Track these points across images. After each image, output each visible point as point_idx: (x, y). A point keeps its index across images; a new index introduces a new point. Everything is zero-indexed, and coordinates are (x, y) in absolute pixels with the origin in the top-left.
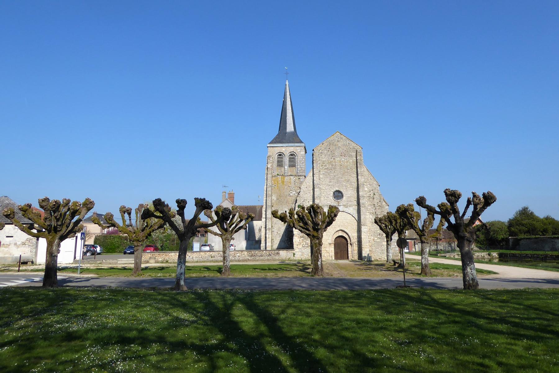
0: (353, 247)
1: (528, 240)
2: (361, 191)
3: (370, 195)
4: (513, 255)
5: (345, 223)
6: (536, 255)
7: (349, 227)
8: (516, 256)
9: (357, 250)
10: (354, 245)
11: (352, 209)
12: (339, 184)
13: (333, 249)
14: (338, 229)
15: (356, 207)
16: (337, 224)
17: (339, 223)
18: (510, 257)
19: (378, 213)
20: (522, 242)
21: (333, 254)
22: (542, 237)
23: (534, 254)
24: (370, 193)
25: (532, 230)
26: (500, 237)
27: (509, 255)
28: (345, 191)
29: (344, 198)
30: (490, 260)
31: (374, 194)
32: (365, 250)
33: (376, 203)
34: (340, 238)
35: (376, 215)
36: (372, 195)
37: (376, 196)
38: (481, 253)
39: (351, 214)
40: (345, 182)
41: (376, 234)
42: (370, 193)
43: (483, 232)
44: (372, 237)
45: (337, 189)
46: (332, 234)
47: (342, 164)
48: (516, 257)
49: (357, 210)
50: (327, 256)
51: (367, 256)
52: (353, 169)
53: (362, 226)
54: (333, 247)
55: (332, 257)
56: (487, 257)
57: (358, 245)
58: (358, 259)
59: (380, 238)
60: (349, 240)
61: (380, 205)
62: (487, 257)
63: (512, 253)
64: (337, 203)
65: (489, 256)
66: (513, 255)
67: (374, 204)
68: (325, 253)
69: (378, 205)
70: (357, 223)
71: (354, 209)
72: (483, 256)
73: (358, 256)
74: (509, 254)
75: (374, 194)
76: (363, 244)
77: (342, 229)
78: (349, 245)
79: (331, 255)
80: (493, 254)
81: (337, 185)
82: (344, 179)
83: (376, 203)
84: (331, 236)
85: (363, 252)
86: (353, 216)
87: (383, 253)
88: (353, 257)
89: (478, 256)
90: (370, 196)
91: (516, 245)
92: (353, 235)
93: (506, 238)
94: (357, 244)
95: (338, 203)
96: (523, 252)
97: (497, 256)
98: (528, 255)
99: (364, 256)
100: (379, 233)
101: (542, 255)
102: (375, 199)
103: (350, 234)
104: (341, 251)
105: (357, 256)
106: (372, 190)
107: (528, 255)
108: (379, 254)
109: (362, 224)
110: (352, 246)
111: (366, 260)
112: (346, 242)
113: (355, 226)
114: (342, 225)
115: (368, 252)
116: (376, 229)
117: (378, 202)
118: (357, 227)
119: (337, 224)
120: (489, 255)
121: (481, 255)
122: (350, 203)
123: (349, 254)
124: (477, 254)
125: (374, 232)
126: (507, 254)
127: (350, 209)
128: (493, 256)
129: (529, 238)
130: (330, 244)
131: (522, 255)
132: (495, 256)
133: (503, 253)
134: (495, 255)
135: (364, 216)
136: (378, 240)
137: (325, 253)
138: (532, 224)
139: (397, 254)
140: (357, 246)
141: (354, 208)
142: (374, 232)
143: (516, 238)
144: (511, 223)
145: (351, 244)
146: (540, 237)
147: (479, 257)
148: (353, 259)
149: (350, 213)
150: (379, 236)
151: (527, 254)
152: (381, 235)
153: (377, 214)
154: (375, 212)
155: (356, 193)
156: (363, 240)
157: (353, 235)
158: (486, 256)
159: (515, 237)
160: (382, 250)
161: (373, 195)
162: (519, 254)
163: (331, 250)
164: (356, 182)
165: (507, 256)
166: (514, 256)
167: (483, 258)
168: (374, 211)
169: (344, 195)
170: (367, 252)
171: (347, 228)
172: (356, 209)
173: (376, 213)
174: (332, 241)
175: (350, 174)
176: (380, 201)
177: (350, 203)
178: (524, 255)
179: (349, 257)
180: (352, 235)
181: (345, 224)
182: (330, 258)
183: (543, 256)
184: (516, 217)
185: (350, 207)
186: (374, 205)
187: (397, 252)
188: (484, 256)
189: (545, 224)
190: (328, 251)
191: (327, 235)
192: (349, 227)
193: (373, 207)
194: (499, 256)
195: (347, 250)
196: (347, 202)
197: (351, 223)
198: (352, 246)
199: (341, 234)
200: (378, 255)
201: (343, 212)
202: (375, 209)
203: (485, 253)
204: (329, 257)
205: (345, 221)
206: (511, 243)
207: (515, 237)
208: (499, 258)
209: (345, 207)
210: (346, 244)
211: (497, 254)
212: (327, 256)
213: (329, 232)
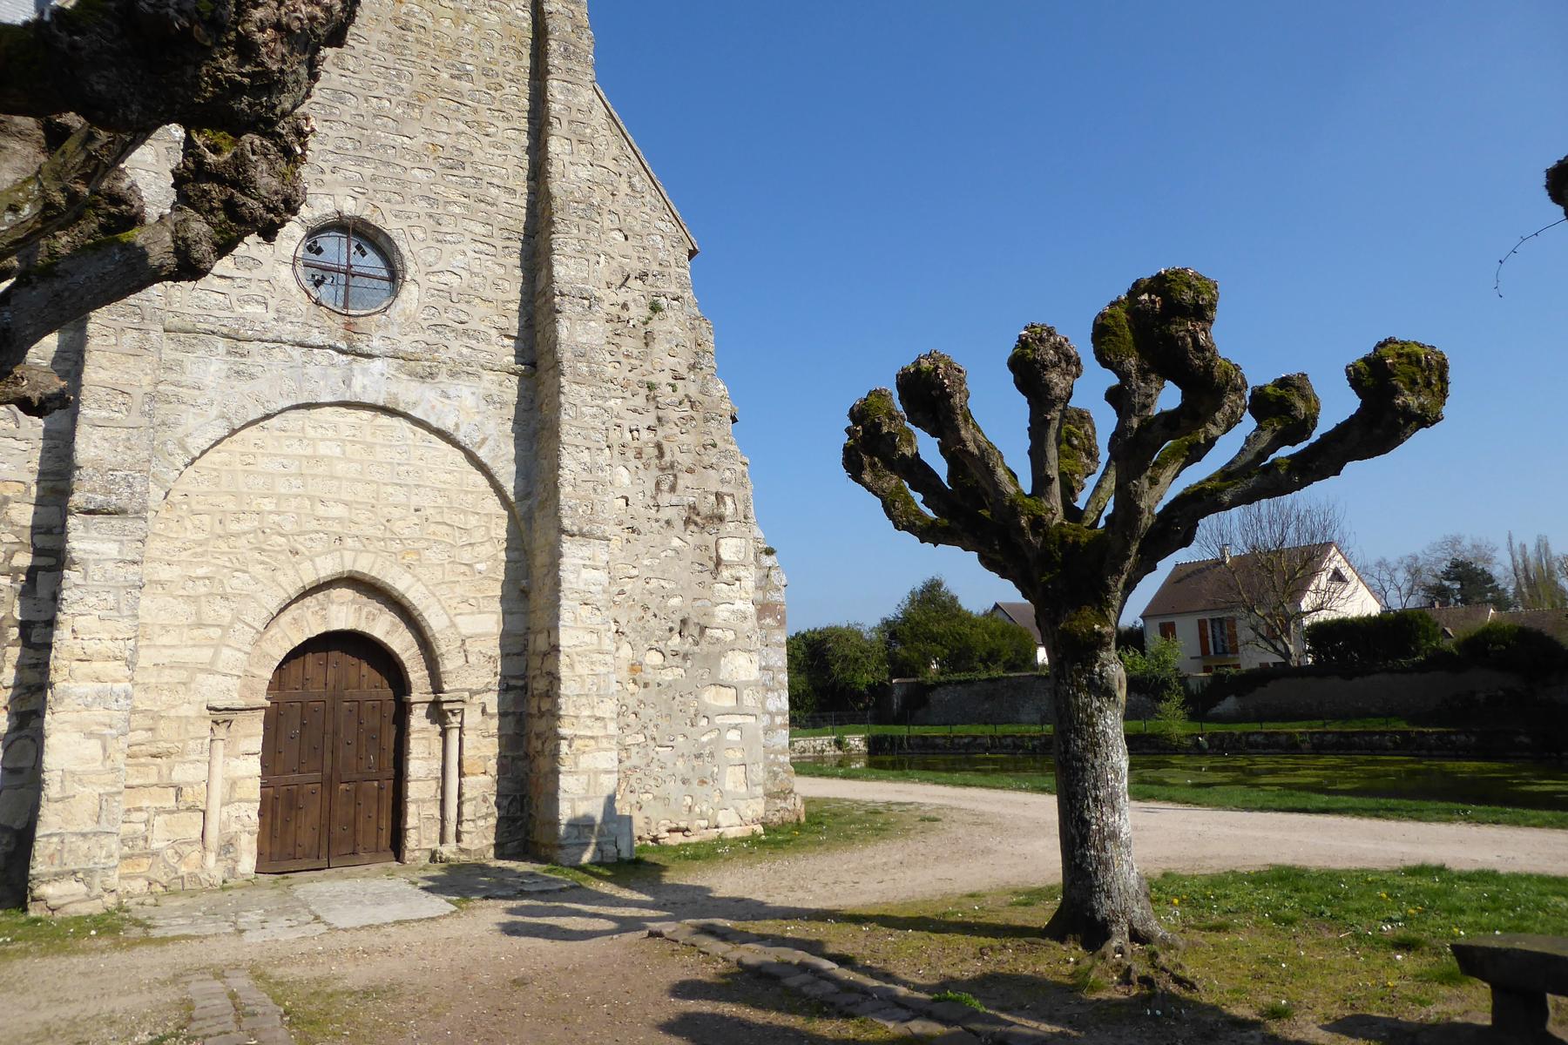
0: (454, 736)
1: (959, 688)
2: (567, 250)
3: (625, 306)
4: (921, 742)
5: (396, 513)
6: (1009, 741)
7: (432, 556)
8: (936, 746)
9: (492, 766)
10: (472, 717)
11: (469, 401)
12: (368, 171)
13: (254, 766)
14: (328, 568)
15: (510, 390)
16: (314, 525)
17: (338, 511)
18: (910, 751)
19: (679, 457)
20: (934, 697)
21: (250, 813)
22: (1015, 677)
23: (1005, 737)
24: (623, 296)
25: (959, 657)
26: (865, 679)
27: (908, 743)
28: (419, 234)
29: (411, 295)
30: (840, 765)
31: (655, 308)
32: (585, 762)
33: (664, 379)
34: (335, 655)
35: (663, 469)
36: (638, 312)
37: (665, 326)
38: (815, 741)
39: (460, 436)
40: (429, 163)
41: (653, 622)
42: (623, 296)
43: (800, 665)
44: (626, 651)
45: (350, 208)
46: (257, 617)
47: (408, 13)
48: (934, 748)
49: (511, 412)
50: (178, 845)
51: (599, 819)
52: (506, 84)
53: (568, 546)
54: (256, 744)
55: (228, 847)
56: (831, 751)
57: (502, 715)
58: (499, 855)
59: (685, 657)
60: (417, 675)
61: (693, 391)
62: (832, 753)
63: (917, 737)
64: (341, 332)
65: (840, 749)
66: (921, 742)
67: (653, 379)
68: (160, 811)
69: (681, 393)
70: (504, 523)
71: (488, 399)
72: (819, 748)
73: (500, 820)
74: (909, 738)
75: (655, 308)
76: (566, 706)
77: (365, 565)
78: (418, 720)
79: (224, 825)
80: (852, 742)
81: (351, 169)
82: (423, 138)
83: (664, 379)
84: (244, 636)
85: (565, 782)
86: (482, 454)
87: (703, 782)
88: (451, 829)
89: (804, 752)
90: (625, 315)
91: (918, 702)
92: (467, 625)
93: (881, 684)
94: (493, 708)
95: (348, 326)
96: (960, 730)
97: (862, 747)
98: (979, 741)
99: (573, 824)
100: (677, 618)
101: (1032, 738)
102: (660, 347)
103: (435, 621)
104: (329, 783)
105: (493, 821)
106: (642, 276)
107: (979, 741)
108: (673, 787)
109: (566, 523)
110: (444, 734)
111: (586, 857)
112: (388, 693)
113: (487, 549)
114: (370, 532)
115: (608, 783)
116: (654, 583)
117: (683, 371)
118: (503, 556)
119: (314, 525)
120: (839, 744)
121: (814, 748)
122: (457, 348)
123: (412, 809)
124: (802, 743)
125: (646, 608)
126: (901, 738)
127: (452, 392)
128: (851, 750)
129: (966, 681)
130: (222, 716)
131: (956, 741)
132: (857, 746)
133: (885, 737)
134: (857, 743)
135: (585, 456)
136: (668, 676)
137: (160, 811)
138: (958, 634)
139: (783, 776)
140: (495, 723)
141: (494, 389)
142: (646, 608)
143: (918, 683)
144: (893, 631)
145: (437, 713)
146: (1008, 677)
147: (807, 754)
148: (449, 850)
149: (447, 425)
150: (676, 639)
151: (975, 738)
152: (696, 633)
153: (667, 458)
154: (659, 446)
155: (518, 273)
156: (572, 666)
157: (465, 631)
158: (828, 749)
159: (912, 680)
160: (698, 756)
161: (647, 312)
162: (945, 737)
163: (233, 784)
164: (522, 188)
165: (901, 746)
166: (926, 744)
167: (820, 757)
168: (645, 435)
169: (411, 270)
170: (604, 778)
171: (410, 558)
172: (503, 404)
173: (661, 455)
174: (248, 689)
175: (476, 111)
176: (692, 367)
177: (457, 348)
178: (966, 741)
179: (412, 840)
180: (453, 625)
181: (398, 526)
182: (211, 859)
183: (1035, 743)
184: (905, 612)
185: (453, 374)
186: (651, 387)
187: (781, 765)
188: (823, 751)
189: (992, 635)
190: (189, 796)
191: (200, 625)
192: (432, 556)
193: (640, 401)
194: (869, 747)
195: (391, 772)
196: (431, 337)
197: (458, 520)
198: (444, 734)
199: (345, 612)
200: (666, 800)
201: (384, 420)
202: (653, 422)
203: (826, 739)
204: (196, 856)
205: (401, 498)
206: (896, 701)
207: (912, 680)
208: (869, 753)
209: (412, 374)
210: (391, 708)
211: (863, 739)
212: (178, 845)
213: (225, 597)
